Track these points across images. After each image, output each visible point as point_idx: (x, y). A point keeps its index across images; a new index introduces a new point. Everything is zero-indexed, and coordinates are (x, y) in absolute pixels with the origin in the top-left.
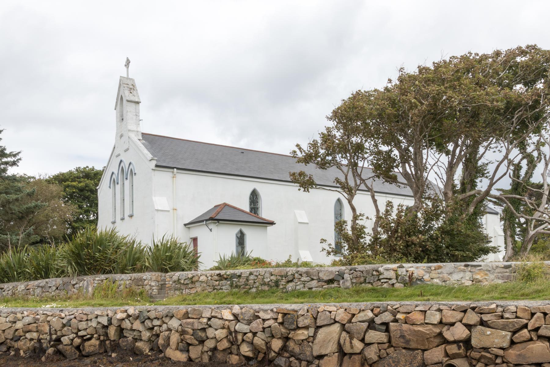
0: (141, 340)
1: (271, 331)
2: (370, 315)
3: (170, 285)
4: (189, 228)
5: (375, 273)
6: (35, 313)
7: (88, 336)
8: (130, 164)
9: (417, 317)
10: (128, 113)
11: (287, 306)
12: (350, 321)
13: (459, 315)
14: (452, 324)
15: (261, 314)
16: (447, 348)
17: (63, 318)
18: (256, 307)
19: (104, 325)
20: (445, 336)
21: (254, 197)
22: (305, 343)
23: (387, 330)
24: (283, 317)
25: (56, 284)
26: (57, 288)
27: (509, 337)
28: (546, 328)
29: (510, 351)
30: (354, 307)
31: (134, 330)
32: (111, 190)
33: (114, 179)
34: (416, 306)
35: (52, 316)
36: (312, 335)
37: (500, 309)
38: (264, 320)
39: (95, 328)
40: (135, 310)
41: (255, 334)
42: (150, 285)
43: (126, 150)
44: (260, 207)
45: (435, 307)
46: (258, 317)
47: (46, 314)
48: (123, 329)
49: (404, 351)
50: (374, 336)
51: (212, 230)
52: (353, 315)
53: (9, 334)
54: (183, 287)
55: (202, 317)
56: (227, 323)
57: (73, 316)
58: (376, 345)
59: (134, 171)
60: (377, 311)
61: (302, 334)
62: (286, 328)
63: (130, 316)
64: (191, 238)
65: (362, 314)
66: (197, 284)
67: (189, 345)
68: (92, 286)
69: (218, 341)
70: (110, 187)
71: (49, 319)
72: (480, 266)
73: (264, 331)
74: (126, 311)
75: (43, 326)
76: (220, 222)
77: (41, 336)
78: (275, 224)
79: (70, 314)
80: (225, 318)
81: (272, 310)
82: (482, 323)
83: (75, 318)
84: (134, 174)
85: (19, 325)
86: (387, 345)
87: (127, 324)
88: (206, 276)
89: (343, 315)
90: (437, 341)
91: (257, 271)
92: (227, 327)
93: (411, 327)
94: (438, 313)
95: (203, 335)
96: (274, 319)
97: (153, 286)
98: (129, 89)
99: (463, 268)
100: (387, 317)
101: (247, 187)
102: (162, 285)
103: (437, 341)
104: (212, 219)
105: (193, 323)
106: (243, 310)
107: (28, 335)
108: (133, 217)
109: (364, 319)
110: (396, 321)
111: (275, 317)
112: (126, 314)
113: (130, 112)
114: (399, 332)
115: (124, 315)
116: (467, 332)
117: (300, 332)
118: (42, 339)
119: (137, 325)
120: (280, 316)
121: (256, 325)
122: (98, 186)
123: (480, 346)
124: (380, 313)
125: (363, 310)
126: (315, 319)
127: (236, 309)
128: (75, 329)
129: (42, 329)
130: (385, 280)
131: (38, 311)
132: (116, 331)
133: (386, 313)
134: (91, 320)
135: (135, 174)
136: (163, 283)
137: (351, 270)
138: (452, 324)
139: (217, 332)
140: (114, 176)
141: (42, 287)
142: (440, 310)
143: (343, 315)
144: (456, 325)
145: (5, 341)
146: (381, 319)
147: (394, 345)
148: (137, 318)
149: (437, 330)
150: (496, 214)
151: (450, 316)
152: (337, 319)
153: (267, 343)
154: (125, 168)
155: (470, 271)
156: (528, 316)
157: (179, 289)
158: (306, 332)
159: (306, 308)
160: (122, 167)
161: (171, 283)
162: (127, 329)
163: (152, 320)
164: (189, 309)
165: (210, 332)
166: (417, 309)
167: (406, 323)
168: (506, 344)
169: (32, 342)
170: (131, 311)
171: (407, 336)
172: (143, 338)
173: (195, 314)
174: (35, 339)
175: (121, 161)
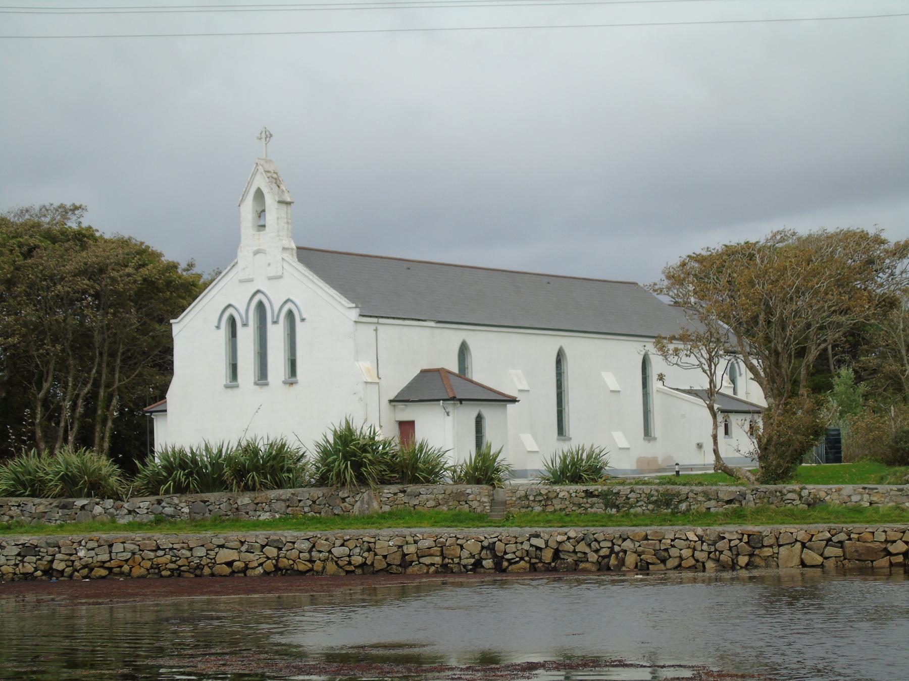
1: (738, 549)
4: (394, 405)
5: (778, 494)
9: (869, 537)
11: (751, 528)
12: (810, 540)
14: (895, 541)
16: (891, 558)
17: (481, 542)
18: (720, 529)
20: (890, 550)
21: (463, 350)
22: (770, 558)
30: (813, 528)
38: (730, 541)
41: (721, 552)
42: (479, 501)
44: (470, 367)
45: (881, 529)
46: (724, 538)
49: (857, 562)
50: (831, 551)
52: (813, 535)
53: (394, 559)
54: (532, 504)
60: (833, 532)
61: (767, 552)
64: (397, 421)
65: (820, 534)
67: (648, 564)
68: (377, 500)
70: (218, 327)
71: (459, 542)
72: (877, 489)
74: (566, 534)
75: (453, 549)
76: (463, 402)
78: (519, 401)
80: (690, 539)
81: (737, 532)
83: (499, 540)
88: (568, 492)
89: (804, 535)
90: (883, 554)
91: (640, 489)
92: (693, 547)
93: (863, 544)
94: (883, 533)
96: (739, 539)
99: (861, 490)
100: (842, 536)
101: (452, 338)
103: (883, 554)
107: (427, 560)
109: (823, 538)
110: (850, 539)
111: (740, 538)
112: (566, 536)
114: (853, 548)
120: (746, 536)
121: (720, 545)
122: (176, 318)
124: (836, 534)
125: (822, 532)
126: (777, 539)
127: (699, 531)
128: (502, 552)
130: (789, 501)
133: (842, 534)
137: (753, 491)
138: (895, 541)
142: (885, 532)
143: (804, 535)
144: (897, 542)
146: (838, 538)
147: (848, 557)
149: (884, 546)
151: (892, 535)
152: (798, 539)
153: (733, 560)
155: (868, 494)
159: (769, 530)
164: (649, 532)
166: (867, 530)
167: (859, 541)
170: (572, 534)
171: (860, 551)
173: (656, 536)
174: (438, 564)
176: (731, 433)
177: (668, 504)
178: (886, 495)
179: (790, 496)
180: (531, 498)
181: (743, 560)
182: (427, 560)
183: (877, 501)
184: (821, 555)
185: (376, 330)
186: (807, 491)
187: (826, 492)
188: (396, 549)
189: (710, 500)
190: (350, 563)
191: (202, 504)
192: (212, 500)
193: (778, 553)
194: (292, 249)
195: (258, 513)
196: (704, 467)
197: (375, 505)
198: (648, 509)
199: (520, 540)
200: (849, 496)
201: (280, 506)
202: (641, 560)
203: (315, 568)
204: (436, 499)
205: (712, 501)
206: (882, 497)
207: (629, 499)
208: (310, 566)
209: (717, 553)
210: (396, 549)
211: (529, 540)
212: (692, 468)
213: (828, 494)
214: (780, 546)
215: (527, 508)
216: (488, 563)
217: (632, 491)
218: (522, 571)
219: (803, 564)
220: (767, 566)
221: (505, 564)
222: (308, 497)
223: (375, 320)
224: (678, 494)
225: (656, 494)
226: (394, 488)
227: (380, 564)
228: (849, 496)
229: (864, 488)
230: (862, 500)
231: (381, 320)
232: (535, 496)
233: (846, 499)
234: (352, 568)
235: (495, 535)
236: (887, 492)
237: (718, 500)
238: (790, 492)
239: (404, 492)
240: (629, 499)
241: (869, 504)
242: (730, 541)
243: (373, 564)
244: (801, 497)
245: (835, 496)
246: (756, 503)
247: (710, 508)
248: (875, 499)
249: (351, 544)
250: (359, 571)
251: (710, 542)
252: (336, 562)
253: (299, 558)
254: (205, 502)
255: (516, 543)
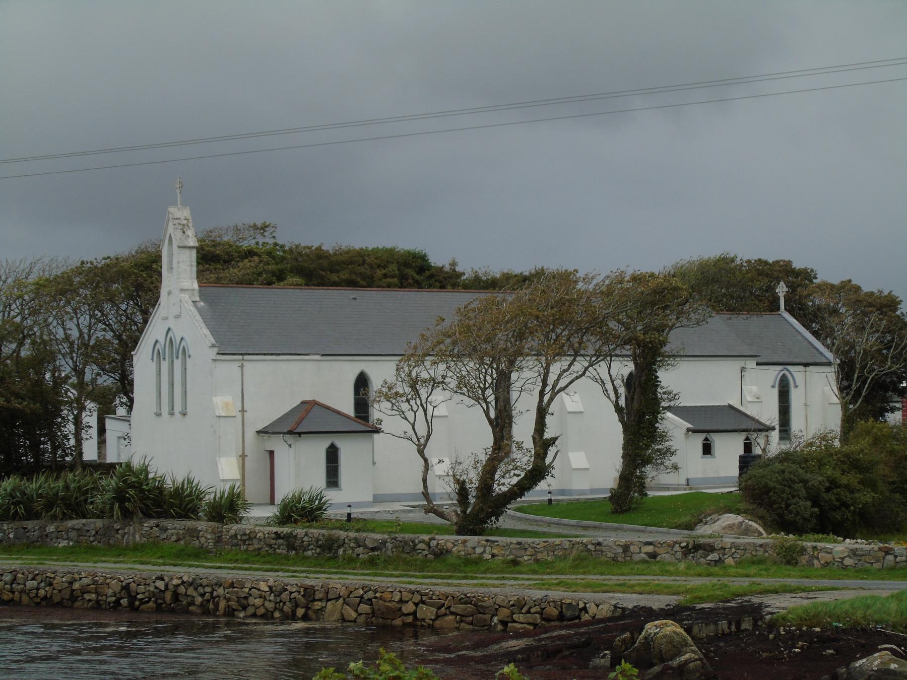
0: (194, 604)
1: (296, 602)
2: (361, 592)
3: (226, 540)
6: (94, 574)
7: (146, 599)
8: (182, 339)
10: (181, 264)
12: (348, 597)
13: (410, 596)
15: (289, 588)
17: (122, 582)
19: (161, 590)
23: (371, 604)
24: (304, 591)
25: (96, 528)
26: (97, 533)
27: (434, 612)
28: (454, 607)
29: (437, 621)
31: (189, 595)
32: (154, 365)
33: (158, 350)
34: (388, 588)
35: (111, 578)
36: (324, 606)
37: (431, 593)
38: (291, 593)
39: (153, 592)
40: (189, 577)
43: (178, 317)
46: (286, 590)
47: (105, 576)
48: (179, 594)
51: (292, 446)
52: (351, 592)
55: (244, 587)
56: (263, 593)
57: (132, 580)
58: (364, 615)
59: (188, 352)
61: (318, 605)
62: (307, 600)
63: (185, 583)
65: (356, 592)
66: (255, 541)
67: (235, 610)
69: (257, 608)
71: (108, 581)
72: (498, 542)
73: (290, 601)
77: (100, 598)
79: (129, 577)
80: (262, 589)
81: (297, 585)
82: (423, 602)
83: (134, 582)
84: (187, 356)
85: (76, 586)
86: (371, 615)
87: (182, 590)
88: (263, 533)
93: (384, 603)
94: (399, 593)
95: (246, 602)
97: (209, 539)
98: (181, 227)
99: (484, 542)
101: (350, 370)
102: (218, 537)
104: (290, 432)
105: (238, 592)
106: (276, 583)
107: (87, 597)
108: (186, 416)
110: (376, 598)
113: (183, 262)
115: (179, 582)
116: (414, 607)
117: (316, 603)
118: (100, 600)
119: (191, 591)
123: (421, 618)
126: (327, 593)
129: (102, 590)
131: (96, 573)
132: (172, 595)
134: (149, 584)
135: (189, 356)
136: (219, 535)
138: (407, 602)
139: (256, 601)
140: (158, 346)
141: (78, 530)
145: (60, 602)
148: (191, 584)
150: (829, 364)
154: (176, 342)
155: (489, 546)
156: (445, 599)
157: (237, 545)
158: (320, 603)
160: (171, 339)
161: (228, 537)
162: (181, 594)
163: (204, 587)
165: (251, 600)
168: (433, 617)
169: (91, 603)
171: (382, 609)
172: (196, 603)
175: (169, 329)
176: (714, 452)
177: (330, 549)
178: (506, 548)
179: (421, 546)
180: (239, 537)
181: (300, 612)
182: (87, 597)
183: (498, 553)
184: (356, 611)
185: (242, 366)
186: (436, 541)
187: (453, 543)
188: (67, 585)
189: (359, 546)
190: (37, 596)
191: (22, 530)
192: (30, 527)
193: (325, 607)
194: (193, 290)
195: (59, 540)
196: (724, 481)
197: (137, 537)
198: (316, 553)
199: (148, 581)
200: (474, 548)
201: (73, 534)
202: (229, 606)
203: (15, 599)
204: (178, 534)
205: (361, 548)
206: (502, 550)
207: (304, 542)
208: (11, 596)
209: (281, 604)
210: (67, 585)
211: (154, 582)
212: (668, 488)
213: (455, 545)
214: (328, 600)
215: (236, 546)
216: (124, 602)
217: (306, 535)
218: (150, 610)
219: (343, 620)
220: (318, 619)
221: (137, 603)
222: (93, 527)
223: (240, 357)
224: (338, 539)
225: (322, 538)
226: (152, 522)
227: (57, 599)
228: (474, 548)
229: (487, 541)
230: (484, 552)
231: (246, 357)
232: (241, 535)
233: (470, 551)
234: (39, 600)
235: (131, 577)
236: (507, 545)
237: (365, 547)
238: (420, 542)
239: (157, 526)
240: (304, 542)
241: (490, 556)
242: (291, 593)
243: (51, 596)
244: (430, 547)
245: (461, 547)
246: (393, 552)
247: (359, 554)
248: (495, 551)
249: (39, 578)
250: (44, 603)
251: (277, 593)
252: (28, 594)
253: (4, 589)
254: (25, 528)
255: (145, 584)
